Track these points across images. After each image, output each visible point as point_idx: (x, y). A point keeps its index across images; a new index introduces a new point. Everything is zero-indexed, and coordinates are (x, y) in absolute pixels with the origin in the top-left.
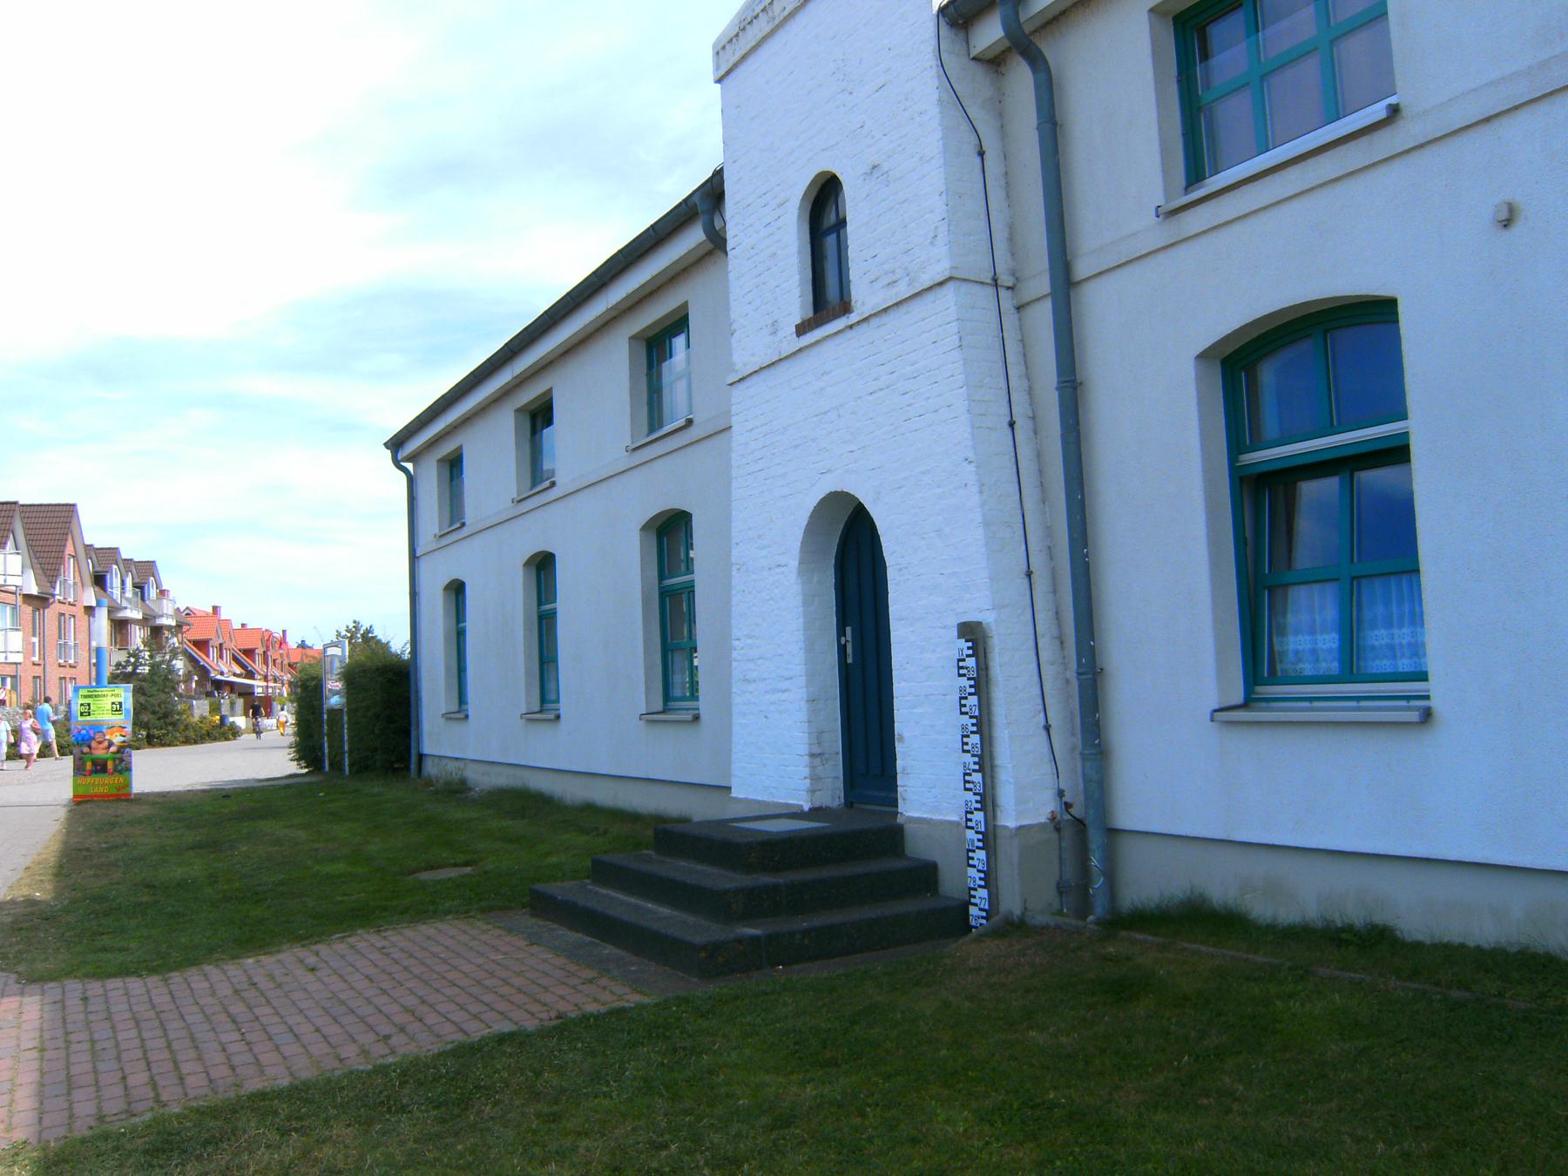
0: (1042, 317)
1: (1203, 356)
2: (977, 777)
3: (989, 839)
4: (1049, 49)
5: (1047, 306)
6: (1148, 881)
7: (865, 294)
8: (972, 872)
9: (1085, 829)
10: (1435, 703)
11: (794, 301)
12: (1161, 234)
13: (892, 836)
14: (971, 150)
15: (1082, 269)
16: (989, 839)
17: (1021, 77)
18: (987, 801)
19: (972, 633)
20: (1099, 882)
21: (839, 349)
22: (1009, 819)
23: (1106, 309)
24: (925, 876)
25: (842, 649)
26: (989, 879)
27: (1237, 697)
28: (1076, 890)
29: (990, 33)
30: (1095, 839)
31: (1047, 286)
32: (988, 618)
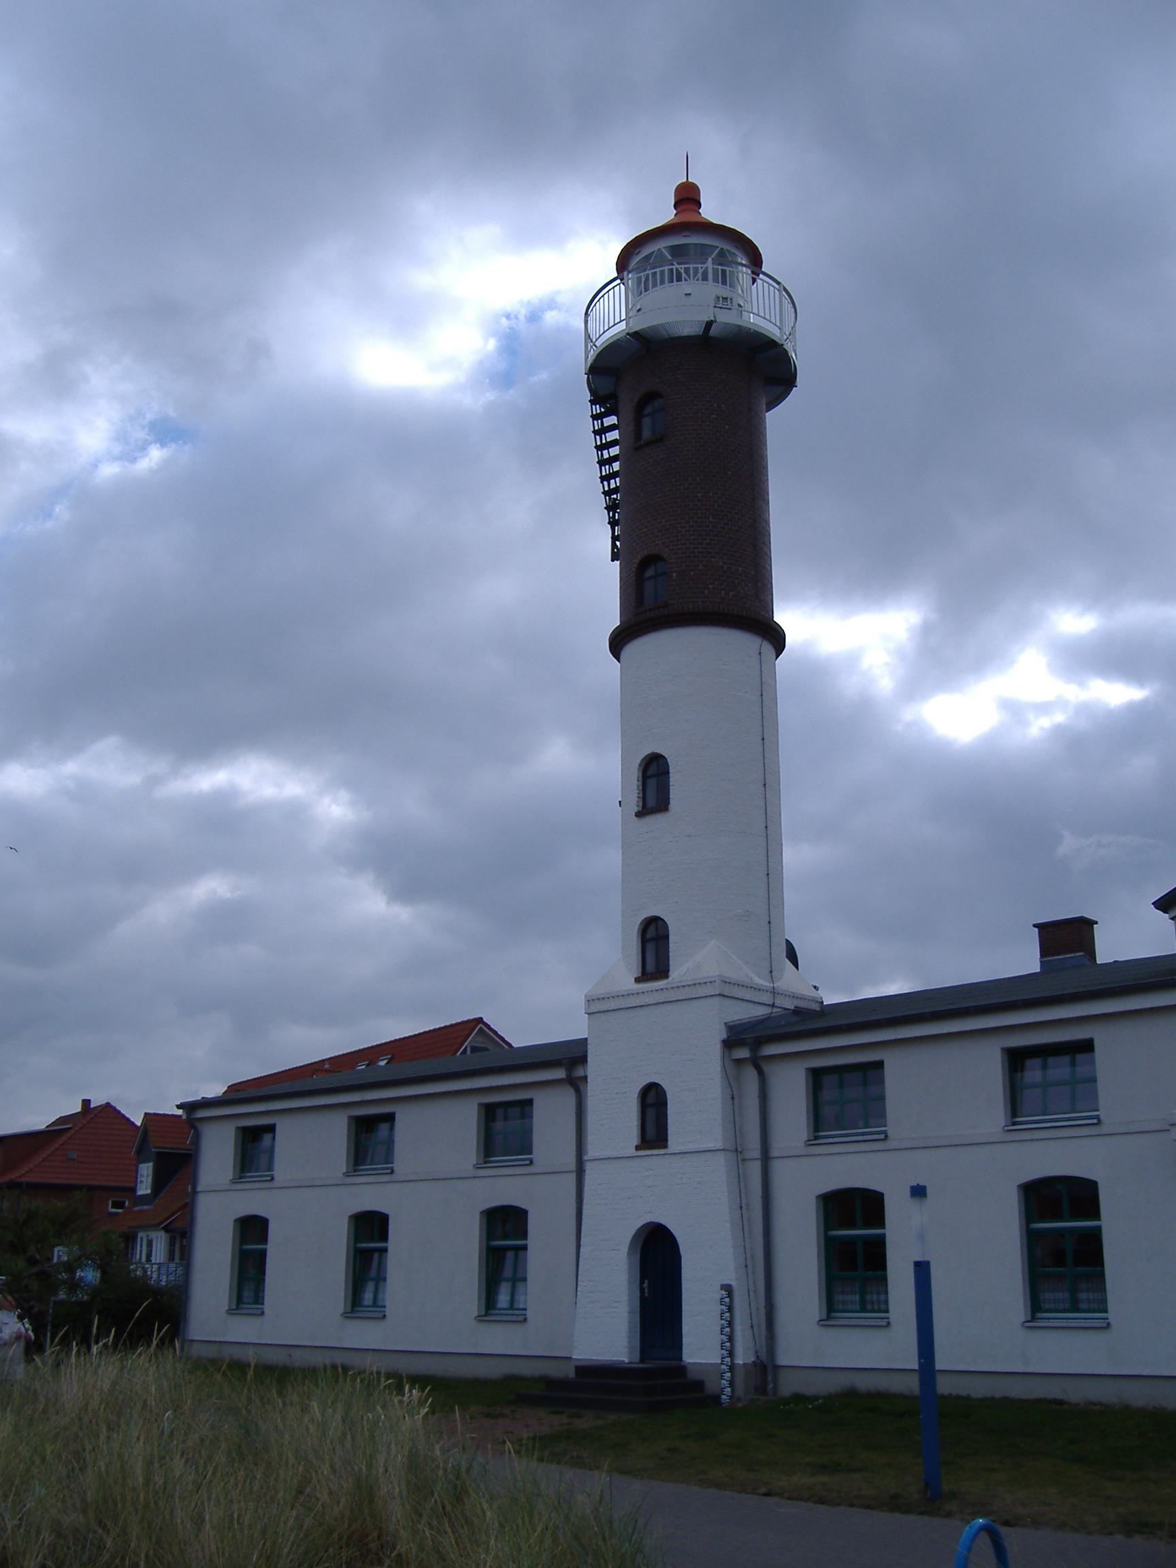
0: (755, 1169)
1: (818, 1197)
2: (728, 1344)
3: (732, 1368)
4: (770, 1069)
5: (758, 1164)
6: (788, 1386)
7: (676, 1139)
8: (723, 1382)
9: (765, 1369)
10: (891, 1321)
11: (632, 1133)
12: (633, 1152)
13: (682, 1370)
14: (729, 1097)
15: (774, 1152)
16: (732, 1368)
17: (751, 1074)
18: (731, 1354)
19: (728, 1289)
20: (771, 1386)
21: (654, 1161)
22: (739, 1361)
23: (783, 1172)
24: (699, 1385)
25: (642, 1290)
26: (732, 1383)
27: (824, 1316)
28: (761, 1389)
29: (743, 1053)
30: (769, 1369)
31: (755, 1159)
32: (734, 1283)
